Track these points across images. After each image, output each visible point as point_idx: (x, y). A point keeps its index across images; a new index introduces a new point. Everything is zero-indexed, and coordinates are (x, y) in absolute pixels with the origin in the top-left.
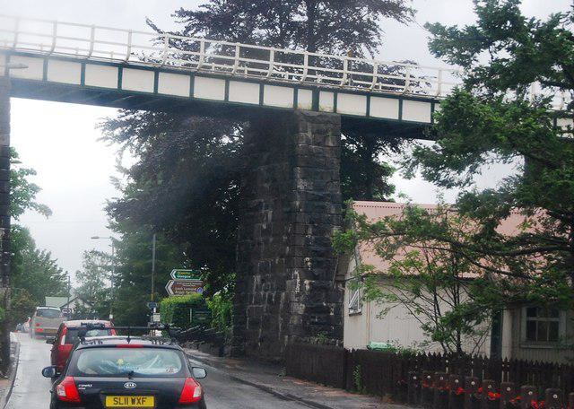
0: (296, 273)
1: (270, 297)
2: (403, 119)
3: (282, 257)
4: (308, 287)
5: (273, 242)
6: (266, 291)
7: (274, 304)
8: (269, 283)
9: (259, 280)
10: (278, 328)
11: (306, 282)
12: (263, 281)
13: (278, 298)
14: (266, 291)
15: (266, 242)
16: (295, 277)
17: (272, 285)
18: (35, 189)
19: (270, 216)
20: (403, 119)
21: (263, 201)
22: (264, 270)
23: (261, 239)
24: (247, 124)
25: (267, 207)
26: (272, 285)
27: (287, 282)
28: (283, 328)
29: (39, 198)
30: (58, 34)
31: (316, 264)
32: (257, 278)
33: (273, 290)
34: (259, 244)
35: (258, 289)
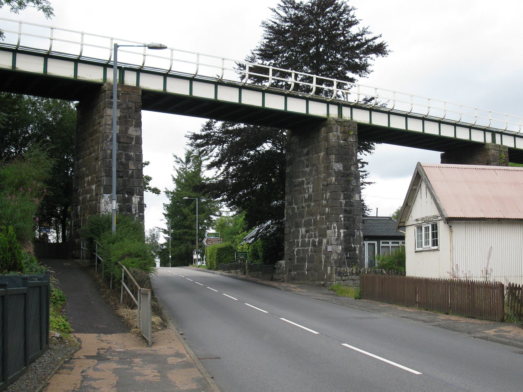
0: (335, 225)
1: (314, 242)
2: (503, 144)
3: (323, 214)
4: (342, 235)
5: (314, 206)
6: (309, 238)
7: (316, 247)
8: (313, 233)
9: (304, 231)
10: (321, 262)
11: (342, 231)
12: (307, 232)
13: (320, 243)
14: (309, 238)
15: (309, 206)
16: (334, 228)
17: (315, 234)
18: (149, 179)
19: (311, 190)
20: (503, 144)
21: (304, 179)
22: (307, 224)
23: (304, 205)
24: (56, 126)
25: (308, 183)
26: (315, 234)
27: (328, 231)
28: (326, 262)
29: (152, 184)
30: (174, 58)
31: (346, 219)
32: (303, 230)
33: (315, 237)
34: (303, 208)
35: (303, 237)
